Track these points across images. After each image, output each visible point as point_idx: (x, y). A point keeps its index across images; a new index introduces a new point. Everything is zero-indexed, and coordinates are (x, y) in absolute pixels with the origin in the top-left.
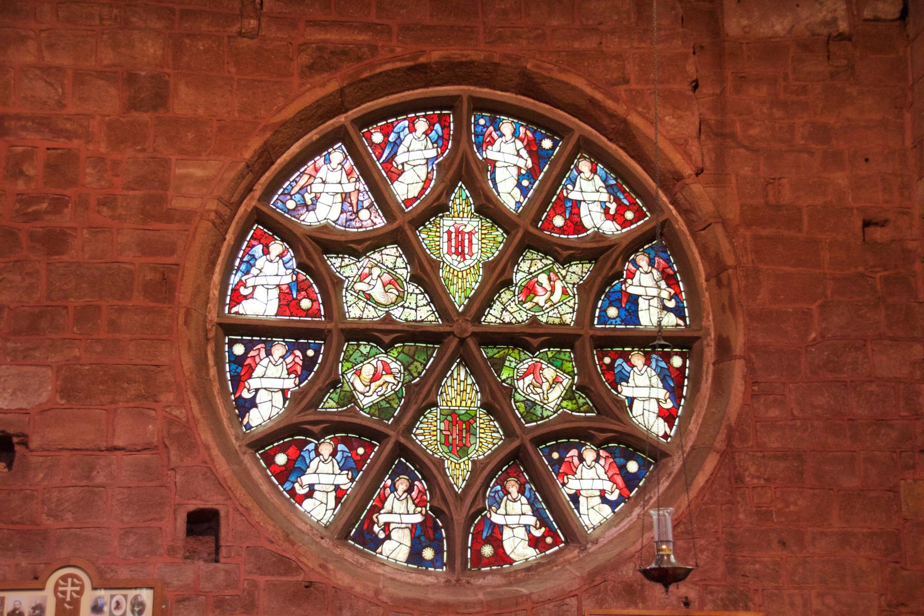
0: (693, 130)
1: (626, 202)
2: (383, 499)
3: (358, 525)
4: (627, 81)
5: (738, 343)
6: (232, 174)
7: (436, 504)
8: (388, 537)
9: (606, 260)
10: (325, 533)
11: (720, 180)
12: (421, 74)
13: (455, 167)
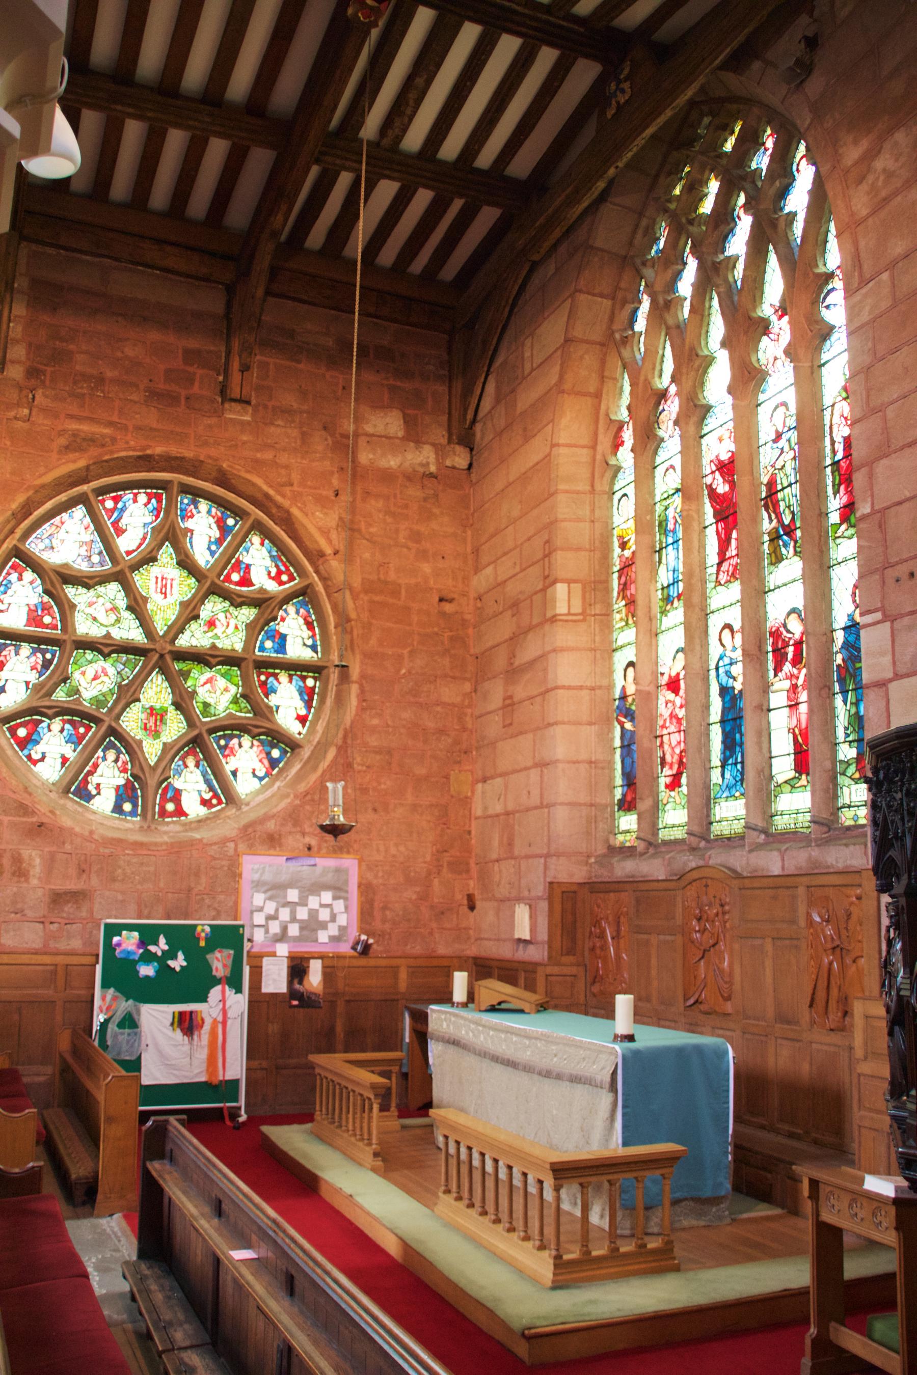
0: (333, 524)
1: (283, 569)
2: (96, 766)
3: (78, 786)
4: (292, 485)
5: (355, 672)
7: (135, 772)
8: (99, 793)
9: (268, 606)
10: (53, 788)
11: (349, 559)
12: (146, 462)
13: (165, 530)
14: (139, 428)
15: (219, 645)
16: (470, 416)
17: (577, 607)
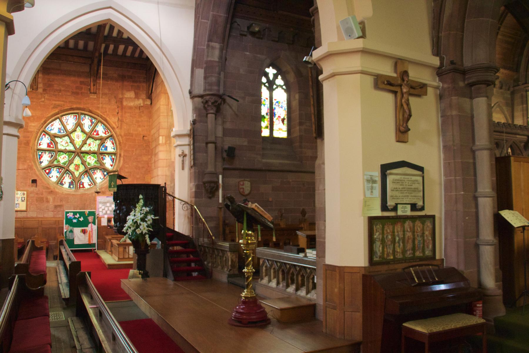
3: (60, 182)
5: (122, 155)
6: (39, 125)
11: (121, 128)
14: (70, 102)
15: (92, 150)
16: (150, 92)
17: (164, 142)
